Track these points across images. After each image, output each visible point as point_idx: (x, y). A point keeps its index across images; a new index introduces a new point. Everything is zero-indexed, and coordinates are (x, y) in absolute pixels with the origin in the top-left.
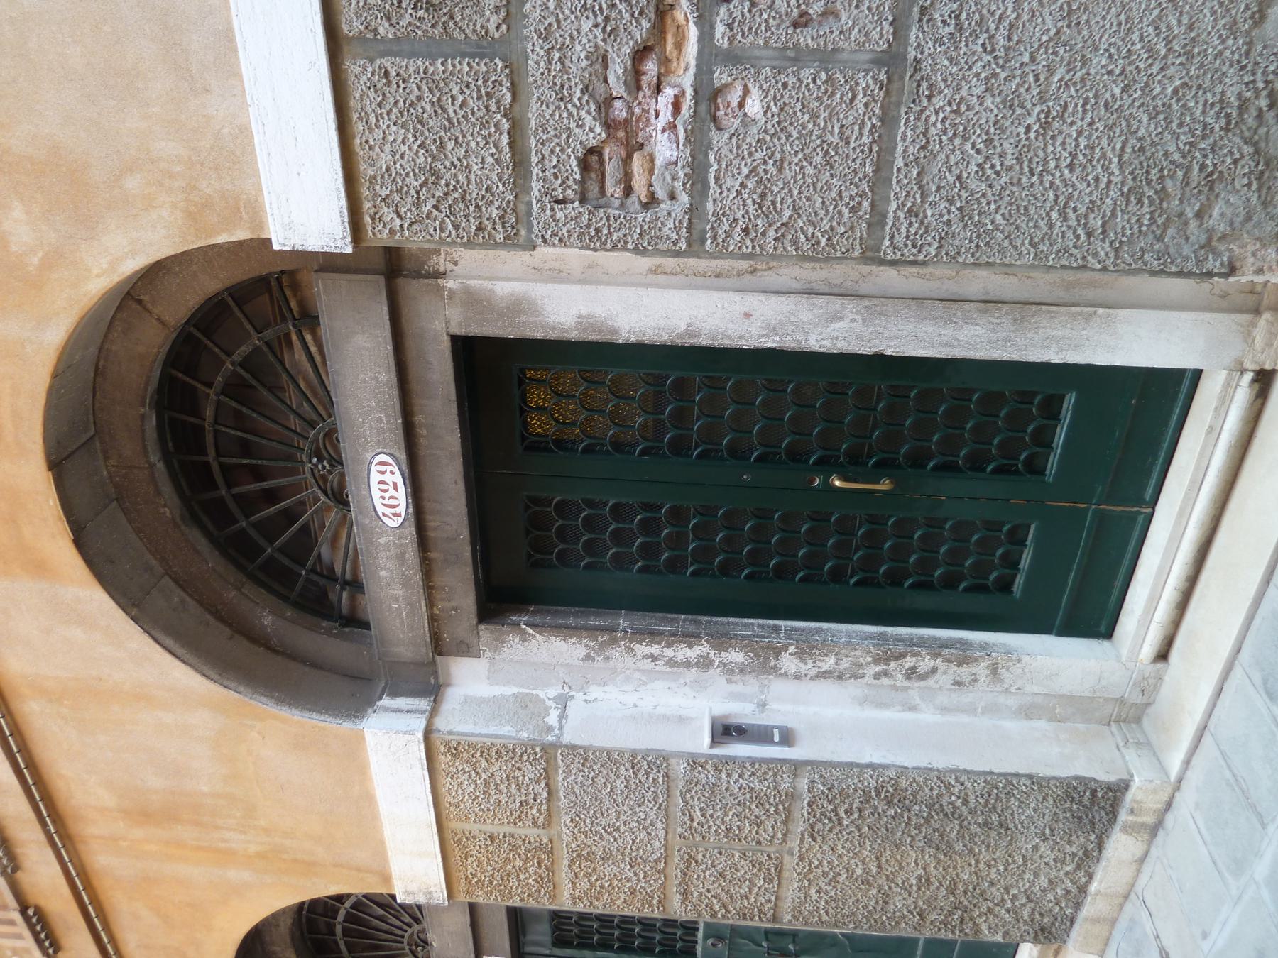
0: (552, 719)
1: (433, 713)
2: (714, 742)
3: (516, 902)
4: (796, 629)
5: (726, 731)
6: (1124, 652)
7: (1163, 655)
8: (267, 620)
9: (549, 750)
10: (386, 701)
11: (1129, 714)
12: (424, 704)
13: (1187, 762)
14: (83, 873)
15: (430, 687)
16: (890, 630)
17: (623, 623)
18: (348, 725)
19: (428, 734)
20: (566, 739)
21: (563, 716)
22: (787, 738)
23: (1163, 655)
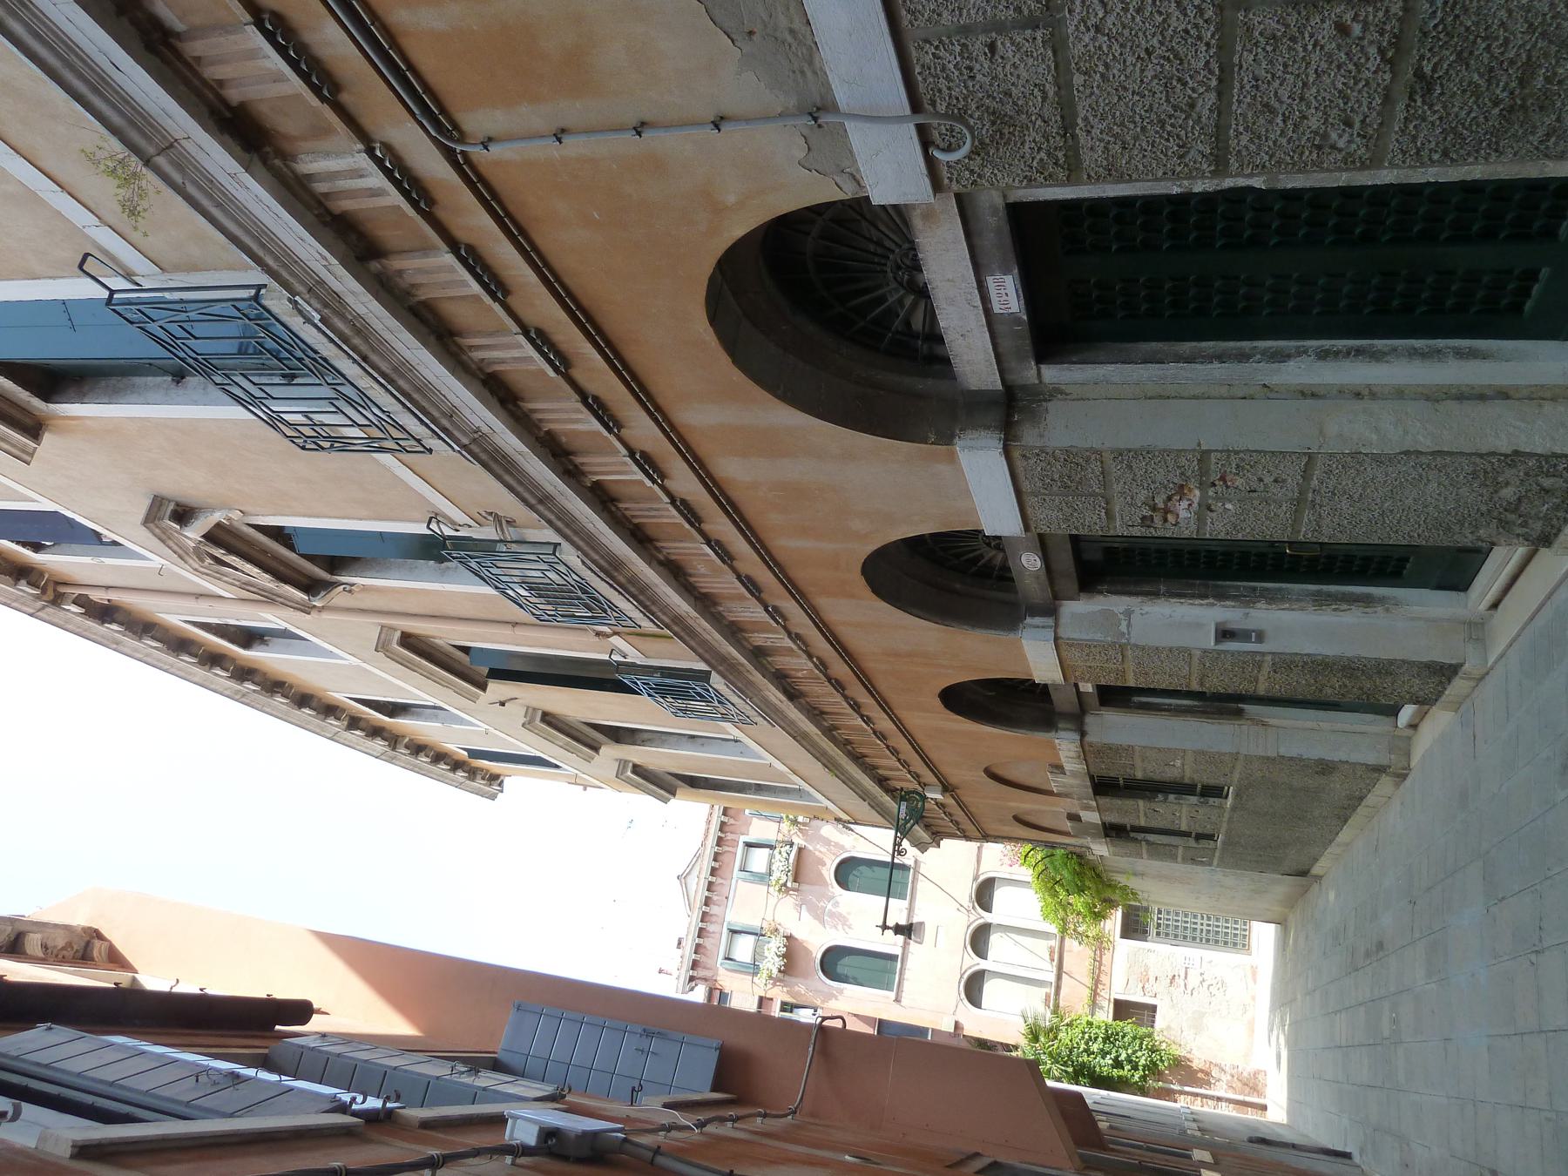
0: (1123, 628)
1: (1056, 626)
2: (1217, 641)
3: (1074, 532)
4: (1267, 589)
5: (1225, 634)
6: (1470, 604)
7: (1495, 606)
8: (958, 586)
9: (1123, 648)
10: (1029, 620)
11: (1476, 630)
12: (1050, 621)
13: (1496, 662)
14: (790, 580)
15: (1051, 611)
16: (1325, 588)
17: (1163, 588)
18: (1012, 636)
19: (1056, 639)
20: (1133, 641)
21: (1129, 625)
22: (1260, 637)
23: (1495, 606)
